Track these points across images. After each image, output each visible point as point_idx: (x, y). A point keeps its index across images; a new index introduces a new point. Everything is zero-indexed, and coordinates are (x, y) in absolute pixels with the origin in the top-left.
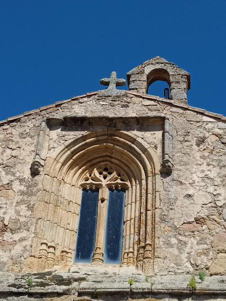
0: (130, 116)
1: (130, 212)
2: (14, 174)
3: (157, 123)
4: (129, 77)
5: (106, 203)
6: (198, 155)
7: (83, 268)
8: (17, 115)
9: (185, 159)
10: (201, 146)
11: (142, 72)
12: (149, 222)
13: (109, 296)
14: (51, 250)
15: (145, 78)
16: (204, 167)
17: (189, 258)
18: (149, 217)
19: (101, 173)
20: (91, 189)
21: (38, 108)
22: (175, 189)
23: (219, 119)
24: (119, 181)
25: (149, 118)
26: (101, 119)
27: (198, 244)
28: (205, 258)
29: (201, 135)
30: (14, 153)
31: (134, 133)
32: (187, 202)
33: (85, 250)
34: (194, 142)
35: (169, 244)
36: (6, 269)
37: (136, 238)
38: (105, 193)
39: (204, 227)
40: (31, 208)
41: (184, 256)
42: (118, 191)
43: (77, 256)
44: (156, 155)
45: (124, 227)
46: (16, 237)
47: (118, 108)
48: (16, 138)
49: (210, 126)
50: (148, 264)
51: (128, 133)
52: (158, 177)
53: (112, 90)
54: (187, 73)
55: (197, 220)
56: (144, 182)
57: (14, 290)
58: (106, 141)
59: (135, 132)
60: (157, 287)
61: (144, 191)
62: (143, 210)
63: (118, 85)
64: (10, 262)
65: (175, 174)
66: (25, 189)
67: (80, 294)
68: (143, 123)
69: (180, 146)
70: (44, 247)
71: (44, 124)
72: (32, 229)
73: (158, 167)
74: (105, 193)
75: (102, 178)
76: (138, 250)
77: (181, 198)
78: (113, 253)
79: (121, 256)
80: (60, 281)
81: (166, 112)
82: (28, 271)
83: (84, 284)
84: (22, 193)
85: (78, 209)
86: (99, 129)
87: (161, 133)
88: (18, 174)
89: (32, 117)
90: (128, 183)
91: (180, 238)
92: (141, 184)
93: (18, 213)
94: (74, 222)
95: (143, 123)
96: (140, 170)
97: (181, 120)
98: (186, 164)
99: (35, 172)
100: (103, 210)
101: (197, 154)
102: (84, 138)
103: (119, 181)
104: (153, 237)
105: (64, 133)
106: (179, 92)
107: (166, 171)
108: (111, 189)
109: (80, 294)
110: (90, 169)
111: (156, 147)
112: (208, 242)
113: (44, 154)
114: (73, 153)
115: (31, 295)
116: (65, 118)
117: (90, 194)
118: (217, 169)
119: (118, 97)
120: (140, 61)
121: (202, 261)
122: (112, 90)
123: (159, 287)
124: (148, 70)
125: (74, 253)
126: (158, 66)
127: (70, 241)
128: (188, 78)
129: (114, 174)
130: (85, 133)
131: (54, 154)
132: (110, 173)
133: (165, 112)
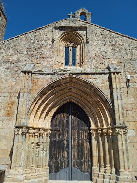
0: (77, 26)
1: (78, 53)
2: (47, 43)
3: (84, 29)
4: (75, 14)
5: (71, 51)
6: (95, 38)
7: (67, 68)
8: (46, 25)
9: (92, 39)
10: (96, 35)
11: (79, 13)
12: (83, 56)
13: (23, 73)
16: (97, 41)
17: (93, 65)
18: (83, 55)
19: (69, 43)
20: (67, 47)
22: (90, 47)
23: (100, 28)
24: (74, 45)
25: (82, 27)
26: (69, 27)
29: (96, 32)
30: (47, 37)
31: (78, 31)
32: (93, 51)
33: (67, 63)
34: (94, 34)
35: (89, 62)
36: (49, 68)
37: (80, 60)
38: (71, 48)
40: (53, 52)
41: (92, 64)
42: (74, 48)
43: (65, 64)
44: (85, 38)
45: (76, 57)
46: (50, 60)
47: (73, 24)
48: (46, 32)
49: (98, 29)
50: (84, 66)
51: (77, 31)
52: (85, 44)
53: (71, 18)
54: (91, 13)
55: (95, 55)
56: (81, 45)
57: (53, 73)
58: (70, 33)
59: (79, 31)
60: (88, 72)
61: (81, 48)
62: (81, 53)
63: (73, 16)
64: (50, 66)
66: (51, 47)
67: (69, 74)
68: (81, 28)
69: (90, 35)
70: (58, 62)
71: (54, 28)
72: (54, 58)
73: (85, 41)
74: (71, 48)
75: (70, 44)
76: (81, 63)
77: (91, 50)
78: (74, 64)
79: (76, 64)
80: (64, 71)
81: (86, 25)
82: (54, 68)
83: (70, 72)
84: (50, 48)
85: (64, 53)
86: (69, 30)
87: (85, 32)
88: (48, 43)
89: (50, 26)
91: (91, 60)
92: (80, 46)
93: (50, 53)
94: (64, 56)
95: (81, 28)
96: (80, 42)
97: (91, 28)
98: (92, 40)
99: (53, 42)
100: (71, 53)
102: (65, 33)
103: (74, 45)
104: (85, 60)
105: (59, 31)
106: (89, 19)
107: (87, 42)
108: (72, 47)
109: (69, 74)
110: (66, 42)
111: (84, 36)
113: (55, 37)
114: (62, 37)
115: (58, 74)
116: (60, 27)
117: (67, 48)
118: (100, 42)
119: (73, 20)
121: (97, 66)
122: (71, 18)
123: (88, 72)
124: (80, 12)
125: (64, 64)
126: (83, 11)
127: (63, 60)
130: (65, 31)
131: (57, 37)
132: (72, 43)
133: (86, 25)
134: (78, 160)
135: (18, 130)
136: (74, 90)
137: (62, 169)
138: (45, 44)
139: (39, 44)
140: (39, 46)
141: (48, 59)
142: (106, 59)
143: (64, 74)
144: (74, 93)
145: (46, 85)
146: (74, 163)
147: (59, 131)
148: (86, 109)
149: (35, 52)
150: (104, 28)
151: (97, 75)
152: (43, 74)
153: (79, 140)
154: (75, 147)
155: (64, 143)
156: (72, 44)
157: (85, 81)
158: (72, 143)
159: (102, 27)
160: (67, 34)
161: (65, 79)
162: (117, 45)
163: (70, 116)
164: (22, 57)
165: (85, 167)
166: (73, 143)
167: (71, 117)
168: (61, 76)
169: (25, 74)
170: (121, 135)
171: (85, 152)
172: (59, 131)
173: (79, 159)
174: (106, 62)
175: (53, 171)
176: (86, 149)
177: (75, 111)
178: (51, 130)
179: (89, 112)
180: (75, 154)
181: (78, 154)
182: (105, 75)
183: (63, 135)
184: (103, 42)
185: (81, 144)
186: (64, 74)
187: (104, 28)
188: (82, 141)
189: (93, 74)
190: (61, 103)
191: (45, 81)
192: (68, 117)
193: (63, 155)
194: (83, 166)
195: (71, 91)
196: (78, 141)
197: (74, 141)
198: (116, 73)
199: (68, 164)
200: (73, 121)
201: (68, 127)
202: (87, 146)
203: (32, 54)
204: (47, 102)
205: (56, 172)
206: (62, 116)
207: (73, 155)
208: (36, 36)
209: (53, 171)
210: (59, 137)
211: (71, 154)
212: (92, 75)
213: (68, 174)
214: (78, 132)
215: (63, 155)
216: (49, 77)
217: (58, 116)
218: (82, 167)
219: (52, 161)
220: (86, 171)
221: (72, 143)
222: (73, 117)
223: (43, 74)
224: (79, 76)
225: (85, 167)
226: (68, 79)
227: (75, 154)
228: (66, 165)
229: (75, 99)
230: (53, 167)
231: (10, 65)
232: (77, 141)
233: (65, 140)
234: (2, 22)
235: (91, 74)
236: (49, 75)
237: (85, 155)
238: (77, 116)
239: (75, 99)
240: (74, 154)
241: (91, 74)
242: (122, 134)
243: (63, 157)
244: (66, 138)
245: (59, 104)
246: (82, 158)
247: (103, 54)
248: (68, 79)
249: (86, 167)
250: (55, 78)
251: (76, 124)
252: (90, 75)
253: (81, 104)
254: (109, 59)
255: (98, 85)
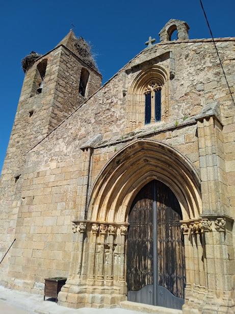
5: (154, 97)
14: (134, 123)
15: (166, 33)
16: (189, 69)
21: (122, 67)
24: (158, 87)
27: (186, 105)
28: (188, 110)
30: (117, 89)
32: (34, 116)
33: (148, 120)
38: (153, 94)
39: (189, 96)
40: (125, 109)
41: (180, 112)
42: (158, 93)
46: (121, 122)
49: (192, 46)
51: (157, 65)
53: (150, 46)
54: (184, 22)
55: (186, 94)
57: (117, 142)
58: (150, 71)
65: (176, 77)
67: (138, 138)
70: (131, 123)
84: (121, 104)
85: (144, 104)
86: (145, 67)
90: (161, 87)
94: (143, 109)
99: (124, 95)
100: (153, 101)
101: (185, 62)
102: (140, 73)
103: (158, 87)
106: (182, 33)
107: (172, 77)
112: (190, 103)
114: (138, 81)
115: (123, 142)
117: (148, 97)
120: (163, 25)
124: (167, 29)
125: (144, 122)
126: (171, 24)
128: (185, 24)
129: (156, 84)
130: (140, 71)
134: (167, 275)
135: (76, 226)
136: (153, 162)
137: (144, 286)
138: (115, 100)
139: (108, 103)
140: (108, 107)
141: (119, 122)
142: (203, 95)
143: (131, 140)
144: (153, 165)
145: (108, 160)
146: (161, 278)
147: (140, 227)
148: (175, 189)
149: (104, 116)
150: (201, 40)
151: (178, 131)
152: (106, 146)
153: (168, 241)
154: (162, 253)
155: (146, 247)
156: (154, 86)
157: (160, 145)
158: (159, 246)
159: (198, 40)
160: (144, 75)
161: (133, 146)
162: (225, 62)
163: (155, 202)
164: (90, 128)
165: (177, 287)
166: (159, 247)
167: (156, 205)
168: (128, 143)
169: (84, 151)
170: (211, 231)
171: (178, 262)
172: (140, 227)
173: (168, 272)
174: (204, 99)
175: (133, 288)
176: (180, 257)
177: (161, 195)
178: (125, 225)
179: (178, 194)
180: (163, 264)
181: (167, 264)
182: (191, 126)
183: (145, 233)
184: (199, 67)
185: (171, 249)
186: (131, 140)
187: (201, 40)
188: (172, 244)
189: (172, 130)
190: (139, 183)
191: (106, 155)
192: (151, 205)
193: (145, 264)
194: (175, 286)
195: (148, 164)
196: (166, 243)
197: (161, 243)
198: (205, 120)
199: (153, 280)
200: (159, 211)
201: (152, 221)
202: (181, 252)
203: (100, 120)
204: (115, 184)
205: (137, 290)
206: (144, 204)
207: (159, 265)
208: (105, 93)
209: (133, 288)
210: (140, 237)
211: (155, 265)
212: (171, 132)
213: (152, 294)
214: (167, 229)
215: (145, 264)
216: (112, 148)
217: (138, 205)
218: (173, 287)
219: (131, 272)
220: (179, 293)
221: (159, 246)
222: (158, 203)
223: (106, 146)
224: (151, 138)
225: (177, 287)
226: (137, 146)
227: (163, 264)
228: (150, 281)
229: (158, 175)
230: (133, 282)
231: (78, 141)
232: (164, 243)
233: (147, 241)
234: (93, 81)
235: (169, 130)
236: (113, 146)
237: (178, 266)
238: (165, 201)
239: (158, 175)
240: (161, 264)
241: (169, 130)
242: (214, 229)
243: (146, 268)
244: (149, 238)
245: (136, 187)
246: (173, 272)
247: (199, 87)
248: (137, 146)
249: (179, 286)
250: (120, 147)
251: (163, 216)
252: (168, 133)
253: (167, 182)
254: (210, 94)
255: (179, 147)
